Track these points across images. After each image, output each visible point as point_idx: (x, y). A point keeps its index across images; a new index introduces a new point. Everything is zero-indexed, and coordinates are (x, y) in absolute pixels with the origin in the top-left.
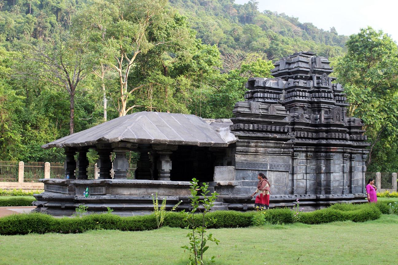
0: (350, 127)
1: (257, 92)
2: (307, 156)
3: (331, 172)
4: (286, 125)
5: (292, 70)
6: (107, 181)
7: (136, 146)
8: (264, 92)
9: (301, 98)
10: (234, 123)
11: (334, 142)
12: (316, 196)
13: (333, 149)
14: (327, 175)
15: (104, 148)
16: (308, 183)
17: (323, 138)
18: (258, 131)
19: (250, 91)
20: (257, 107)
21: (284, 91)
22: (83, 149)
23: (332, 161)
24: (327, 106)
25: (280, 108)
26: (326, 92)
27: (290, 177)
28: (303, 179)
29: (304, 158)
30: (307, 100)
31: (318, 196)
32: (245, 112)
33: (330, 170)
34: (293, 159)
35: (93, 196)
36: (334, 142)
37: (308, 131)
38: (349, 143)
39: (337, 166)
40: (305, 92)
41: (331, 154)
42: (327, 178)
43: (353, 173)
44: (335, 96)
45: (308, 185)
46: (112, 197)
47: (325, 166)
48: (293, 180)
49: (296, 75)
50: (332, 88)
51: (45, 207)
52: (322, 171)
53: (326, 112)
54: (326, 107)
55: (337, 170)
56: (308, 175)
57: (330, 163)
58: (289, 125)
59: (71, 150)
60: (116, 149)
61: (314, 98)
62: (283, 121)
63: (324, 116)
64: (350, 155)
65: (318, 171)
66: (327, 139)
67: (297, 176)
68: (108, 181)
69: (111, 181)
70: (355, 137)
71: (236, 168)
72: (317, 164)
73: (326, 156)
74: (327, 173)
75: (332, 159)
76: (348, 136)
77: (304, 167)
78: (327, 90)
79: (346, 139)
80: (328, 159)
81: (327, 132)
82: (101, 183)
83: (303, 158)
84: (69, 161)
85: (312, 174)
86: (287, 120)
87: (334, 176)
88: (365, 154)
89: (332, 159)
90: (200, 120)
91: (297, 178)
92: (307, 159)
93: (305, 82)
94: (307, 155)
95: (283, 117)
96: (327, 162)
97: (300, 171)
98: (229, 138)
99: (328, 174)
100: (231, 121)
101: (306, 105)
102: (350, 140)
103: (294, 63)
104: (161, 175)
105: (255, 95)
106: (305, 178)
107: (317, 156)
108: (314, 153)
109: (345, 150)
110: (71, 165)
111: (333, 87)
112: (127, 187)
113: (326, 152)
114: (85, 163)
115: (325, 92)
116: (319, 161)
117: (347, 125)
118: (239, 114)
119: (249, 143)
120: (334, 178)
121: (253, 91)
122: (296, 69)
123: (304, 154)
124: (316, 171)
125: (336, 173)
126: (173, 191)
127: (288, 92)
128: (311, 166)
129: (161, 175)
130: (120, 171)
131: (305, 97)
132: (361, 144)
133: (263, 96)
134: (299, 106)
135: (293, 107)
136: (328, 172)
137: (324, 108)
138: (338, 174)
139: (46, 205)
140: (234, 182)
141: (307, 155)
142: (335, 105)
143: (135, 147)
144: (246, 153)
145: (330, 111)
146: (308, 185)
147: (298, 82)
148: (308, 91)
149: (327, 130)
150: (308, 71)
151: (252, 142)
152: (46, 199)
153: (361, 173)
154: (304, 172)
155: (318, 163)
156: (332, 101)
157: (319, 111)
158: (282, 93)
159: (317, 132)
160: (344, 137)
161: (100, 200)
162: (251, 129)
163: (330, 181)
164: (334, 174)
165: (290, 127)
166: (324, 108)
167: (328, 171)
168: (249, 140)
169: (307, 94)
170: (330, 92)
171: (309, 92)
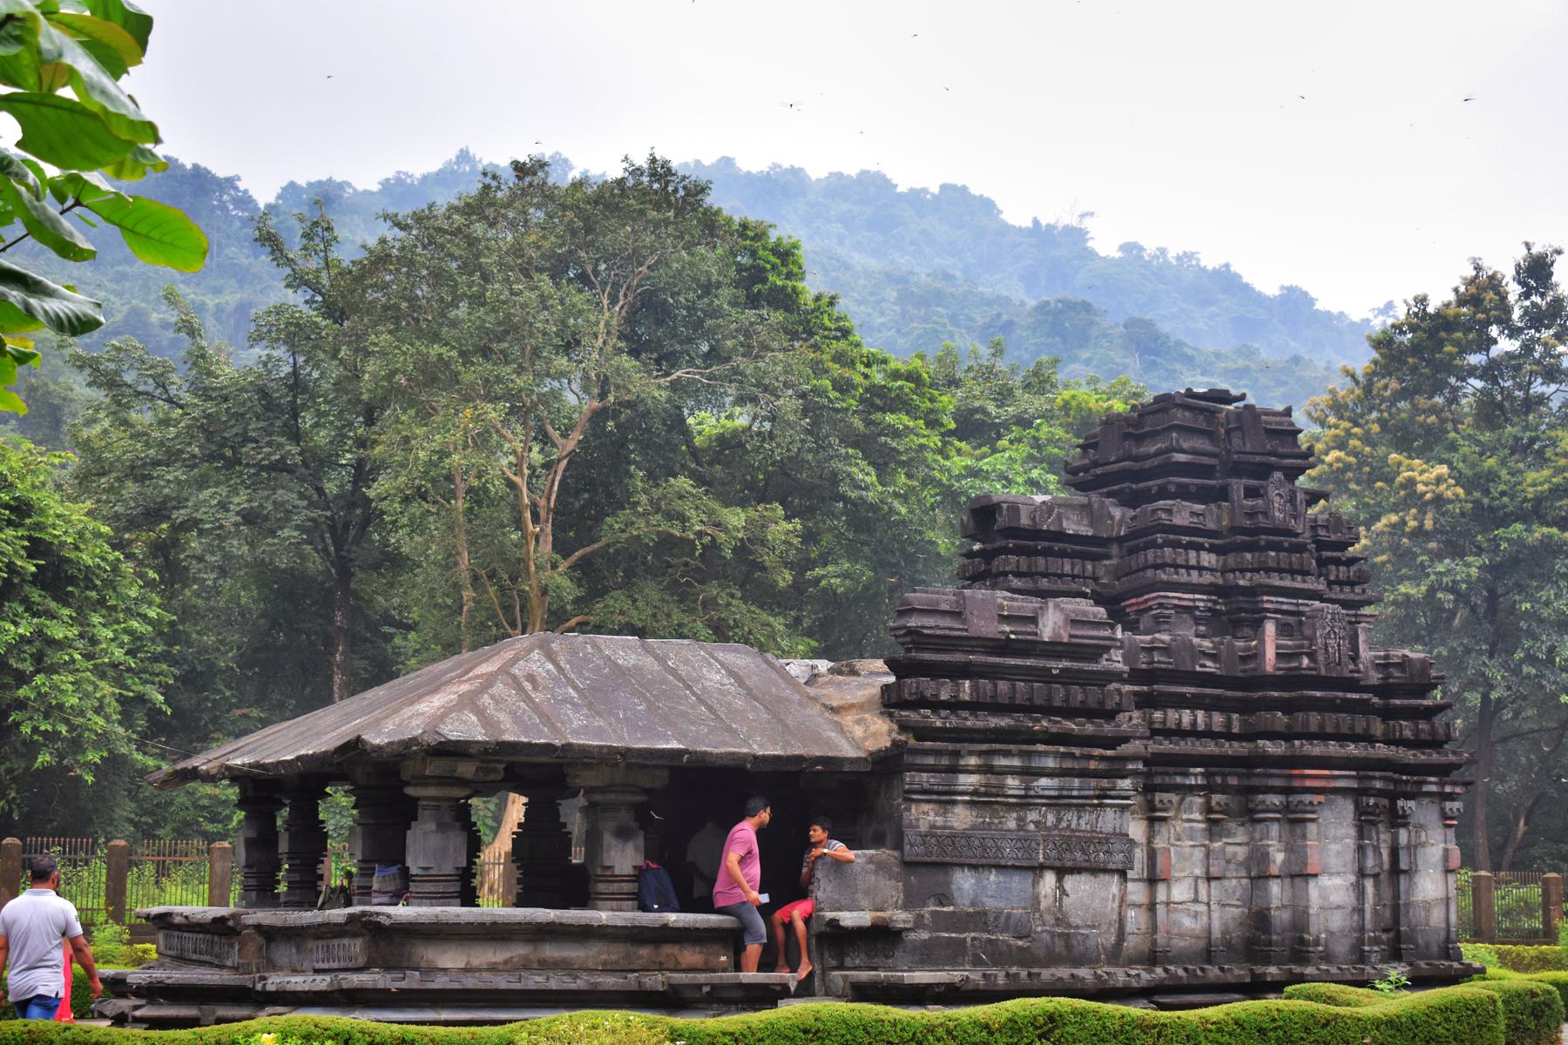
0: (1384, 690)
1: (1006, 551)
2: (1208, 809)
3: (1310, 871)
4: (1110, 682)
5: (1148, 464)
6: (371, 914)
7: (495, 771)
8: (1030, 552)
9: (1195, 573)
10: (898, 678)
11: (1316, 749)
12: (1251, 970)
13: (1313, 777)
14: (1292, 886)
15: (393, 787)
16: (1215, 915)
17: (1272, 736)
18: (996, 708)
19: (976, 547)
20: (990, 609)
21: (1114, 549)
22: (303, 783)
23: (1312, 828)
24: (1286, 603)
25: (1085, 613)
26: (1285, 550)
27: (1137, 892)
28: (1196, 901)
29: (1197, 816)
30: (1207, 578)
31: (1259, 969)
32: (939, 632)
33: (1306, 865)
34: (1152, 821)
35: (319, 978)
36: (1316, 749)
37: (1210, 705)
38: (1382, 750)
39: (1335, 847)
40: (1199, 548)
41: (1307, 798)
42: (1294, 896)
43: (1403, 880)
44: (1322, 563)
45: (1453, 918)
46: (412, 981)
47: (1281, 846)
48: (1152, 907)
49: (1164, 480)
50: (1308, 534)
51: (138, 1021)
52: (1274, 870)
53: (1284, 630)
54: (1285, 607)
55: (1334, 862)
56: (1213, 884)
57: (1304, 837)
58: (1124, 681)
59: (260, 789)
60: (416, 785)
61: (1233, 571)
62: (1103, 664)
63: (1278, 647)
64: (1385, 802)
65: (1258, 874)
66: (1288, 737)
67: (1169, 888)
68: (378, 914)
69: (389, 916)
70: (1406, 729)
71: (908, 859)
72: (1252, 839)
73: (1286, 808)
74: (1292, 876)
75: (1313, 820)
76: (1378, 728)
77: (1199, 854)
78: (1286, 541)
79: (1370, 739)
80: (1295, 820)
81: (1288, 707)
82: (346, 923)
83: (1192, 817)
84: (252, 834)
85: (1234, 882)
86: (1116, 661)
87: (1322, 889)
88: (1453, 800)
89: (1313, 820)
90: (764, 666)
91: (1169, 895)
92: (1209, 821)
93: (1199, 507)
94: (1208, 802)
95: (1095, 652)
96: (1292, 832)
97: (1182, 870)
98: (862, 733)
99: (1298, 881)
100: (886, 668)
101: (1201, 601)
102: (1388, 742)
103: (1153, 435)
104: (602, 887)
105: (998, 563)
106: (1203, 896)
107: (1251, 806)
108: (1238, 798)
109: (1366, 784)
110: (262, 844)
111: (1314, 528)
112: (706, 930)
113: (1288, 791)
114: (312, 842)
115: (1277, 547)
116: (1259, 827)
117: (1375, 677)
118: (917, 638)
119: (956, 754)
120: (1324, 897)
121: (989, 547)
122: (1156, 461)
123: (1199, 800)
124: (1249, 870)
125: (1331, 874)
126: (645, 952)
127: (1133, 551)
128: (1230, 849)
129: (602, 887)
130: (431, 872)
131: (1200, 568)
132: (1435, 756)
133: (1029, 567)
134: (1176, 606)
135: (1150, 608)
136: (1300, 875)
137: (1276, 611)
138: (1338, 881)
139: (138, 1013)
140: (901, 918)
141: (1208, 802)
142: (1323, 600)
143: (492, 777)
144: (945, 798)
145: (1300, 623)
146: (1453, 918)
147: (1169, 511)
148: (1211, 545)
149: (1289, 700)
150: (1213, 467)
151: (971, 753)
152: (139, 987)
153: (1439, 876)
154: (1198, 872)
155: (1257, 836)
156: (1311, 584)
157: (1257, 625)
158: (1109, 557)
159: (1245, 707)
160: (1359, 730)
161: (342, 991)
162: (967, 698)
163: (1307, 907)
164: (1324, 881)
165: (1128, 688)
166: (1276, 611)
167: (1295, 869)
168: (958, 746)
169: (1208, 559)
170: (1300, 548)
171: (1212, 549)
